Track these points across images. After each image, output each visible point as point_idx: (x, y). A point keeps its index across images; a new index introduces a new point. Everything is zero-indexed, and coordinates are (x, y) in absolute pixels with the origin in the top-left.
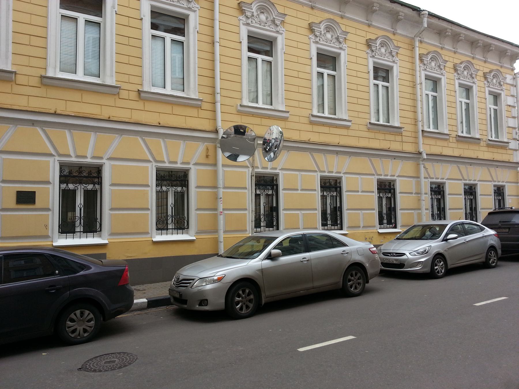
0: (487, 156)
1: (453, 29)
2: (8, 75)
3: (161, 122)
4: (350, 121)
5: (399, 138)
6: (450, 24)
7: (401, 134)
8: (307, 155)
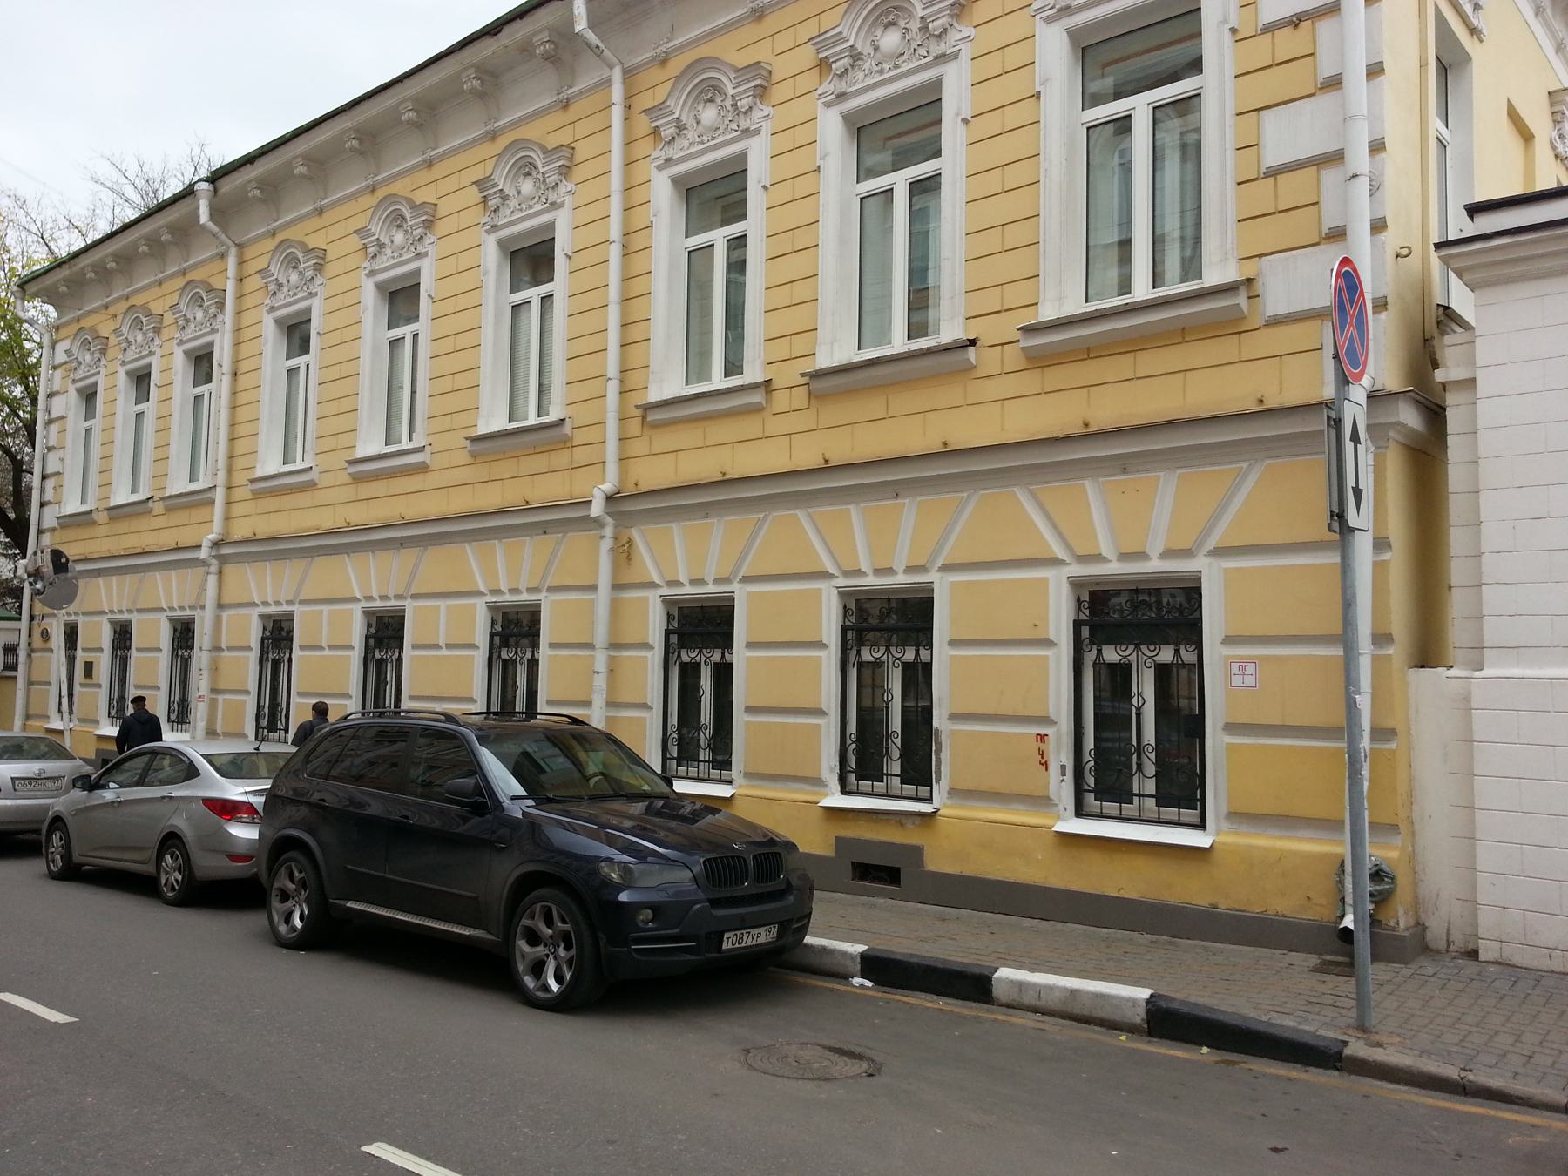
0: (1023, 422)
2: (956, 356)
3: (950, 440)
5: (561, 459)
7: (565, 443)
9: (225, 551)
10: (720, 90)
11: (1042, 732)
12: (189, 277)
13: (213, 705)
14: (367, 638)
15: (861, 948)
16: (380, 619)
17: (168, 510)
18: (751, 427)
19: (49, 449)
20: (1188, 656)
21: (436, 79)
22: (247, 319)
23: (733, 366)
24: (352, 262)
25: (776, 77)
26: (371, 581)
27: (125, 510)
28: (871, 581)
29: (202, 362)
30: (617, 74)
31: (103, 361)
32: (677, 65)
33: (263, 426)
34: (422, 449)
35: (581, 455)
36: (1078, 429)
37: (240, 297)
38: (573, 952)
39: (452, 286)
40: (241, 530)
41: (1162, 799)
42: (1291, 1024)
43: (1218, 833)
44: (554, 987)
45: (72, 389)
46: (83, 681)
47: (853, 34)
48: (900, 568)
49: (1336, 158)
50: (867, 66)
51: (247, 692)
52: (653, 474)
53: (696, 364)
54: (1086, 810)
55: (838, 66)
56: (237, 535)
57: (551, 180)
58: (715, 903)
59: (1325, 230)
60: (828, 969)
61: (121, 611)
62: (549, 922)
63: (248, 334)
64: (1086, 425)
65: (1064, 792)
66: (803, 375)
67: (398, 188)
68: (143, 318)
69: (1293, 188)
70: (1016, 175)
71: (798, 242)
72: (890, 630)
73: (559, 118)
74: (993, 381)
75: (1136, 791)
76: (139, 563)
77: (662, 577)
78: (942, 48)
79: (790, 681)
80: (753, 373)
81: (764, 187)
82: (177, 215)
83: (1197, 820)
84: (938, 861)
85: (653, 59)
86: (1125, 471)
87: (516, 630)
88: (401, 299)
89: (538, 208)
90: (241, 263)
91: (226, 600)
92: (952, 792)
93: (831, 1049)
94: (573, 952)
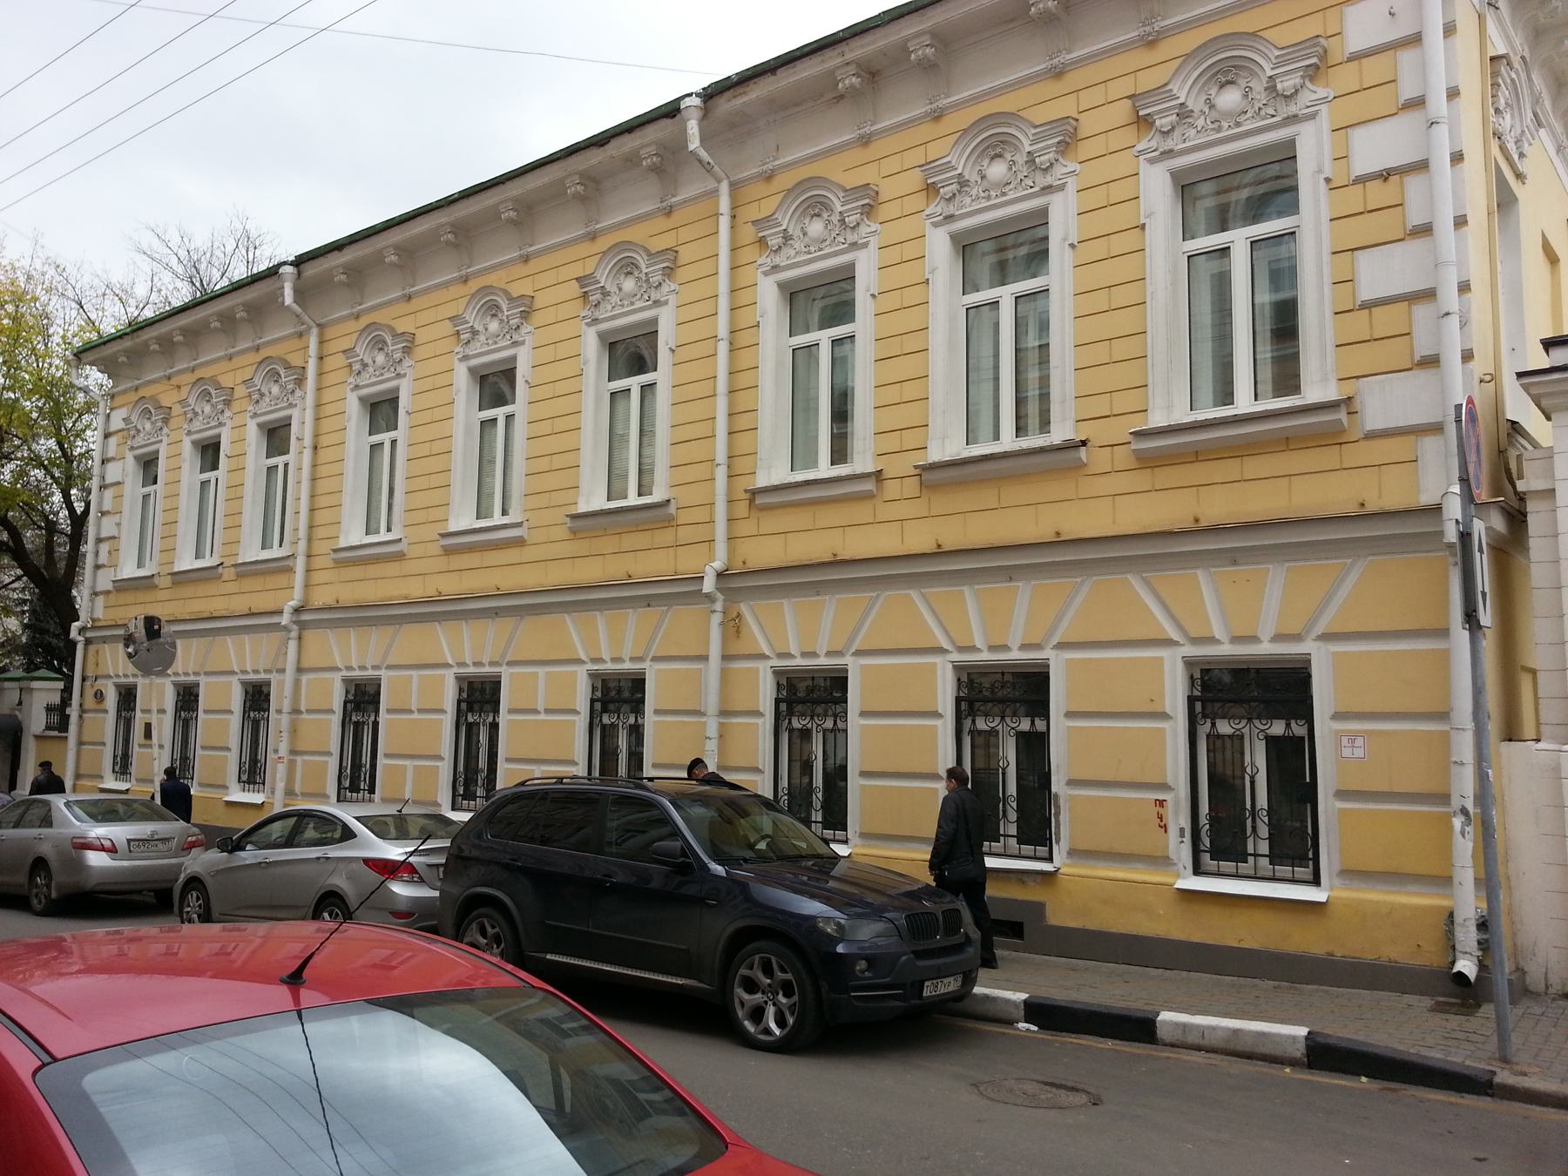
1: (849, 56)
5: (666, 536)
6: (828, 53)
7: (669, 522)
9: (306, 617)
10: (826, 206)
11: (1161, 797)
12: (265, 353)
13: (292, 766)
14: (459, 702)
15: (1024, 996)
16: (470, 683)
17: (240, 576)
18: (861, 512)
19: (103, 514)
21: (546, 180)
22: (328, 395)
23: (840, 453)
24: (442, 346)
25: (882, 198)
26: (469, 648)
27: (192, 575)
28: (985, 656)
29: (276, 436)
30: (724, 188)
31: (166, 430)
32: (785, 181)
33: (346, 499)
34: (519, 525)
35: (685, 534)
36: (1188, 524)
37: (320, 374)
38: (795, 998)
39: (548, 373)
40: (321, 597)
41: (1274, 858)
42: (1439, 1056)
43: (1331, 889)
44: (777, 1032)
45: (130, 457)
46: (143, 741)
47: (961, 163)
48: (1015, 645)
49: (1429, 295)
50: (974, 192)
51: (329, 754)
52: (764, 552)
53: (800, 452)
54: (1203, 868)
55: (946, 191)
56: (318, 603)
57: (655, 279)
58: (919, 955)
59: (1417, 358)
60: (999, 1017)
61: (186, 674)
62: (768, 971)
63: (328, 410)
64: (1197, 521)
65: (1184, 853)
66: (916, 467)
67: (492, 279)
68: (207, 389)
69: (1385, 320)
70: (1122, 296)
71: (906, 346)
72: (1002, 701)
73: (661, 223)
74: (1103, 479)
75: (1250, 850)
76: (211, 626)
77: (773, 649)
78: (1049, 180)
80: (862, 460)
81: (873, 296)
82: (255, 294)
83: (1310, 877)
84: (1058, 916)
85: (759, 175)
86: (1235, 563)
87: (618, 697)
88: (495, 385)
89: (639, 305)
90: (321, 342)
91: (305, 664)
92: (1072, 853)
93: (1047, 1084)
94: (795, 998)
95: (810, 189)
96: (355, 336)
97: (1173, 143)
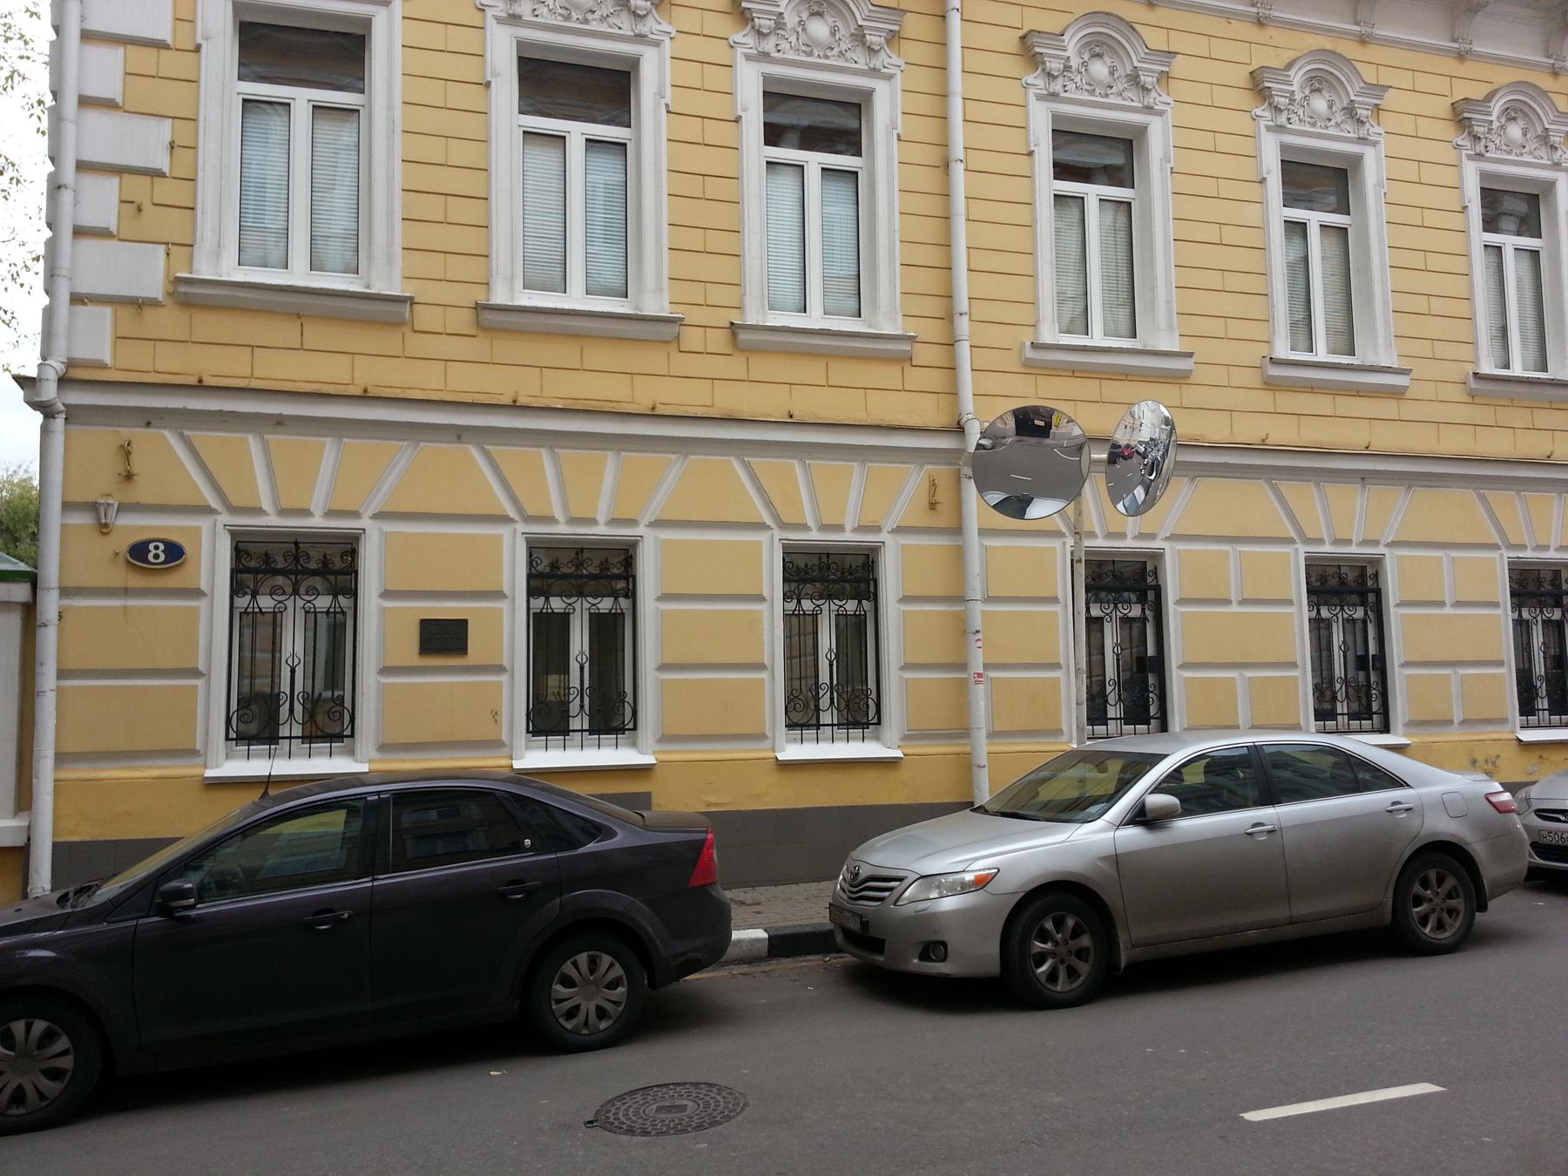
3: (795, 413)
4: (1190, 355)
8: (1469, 495)
20: (624, 603)
41: (1553, 711)
79: (709, 628)
95: (1107, 25)
96: (1071, 18)
97: (769, 45)
